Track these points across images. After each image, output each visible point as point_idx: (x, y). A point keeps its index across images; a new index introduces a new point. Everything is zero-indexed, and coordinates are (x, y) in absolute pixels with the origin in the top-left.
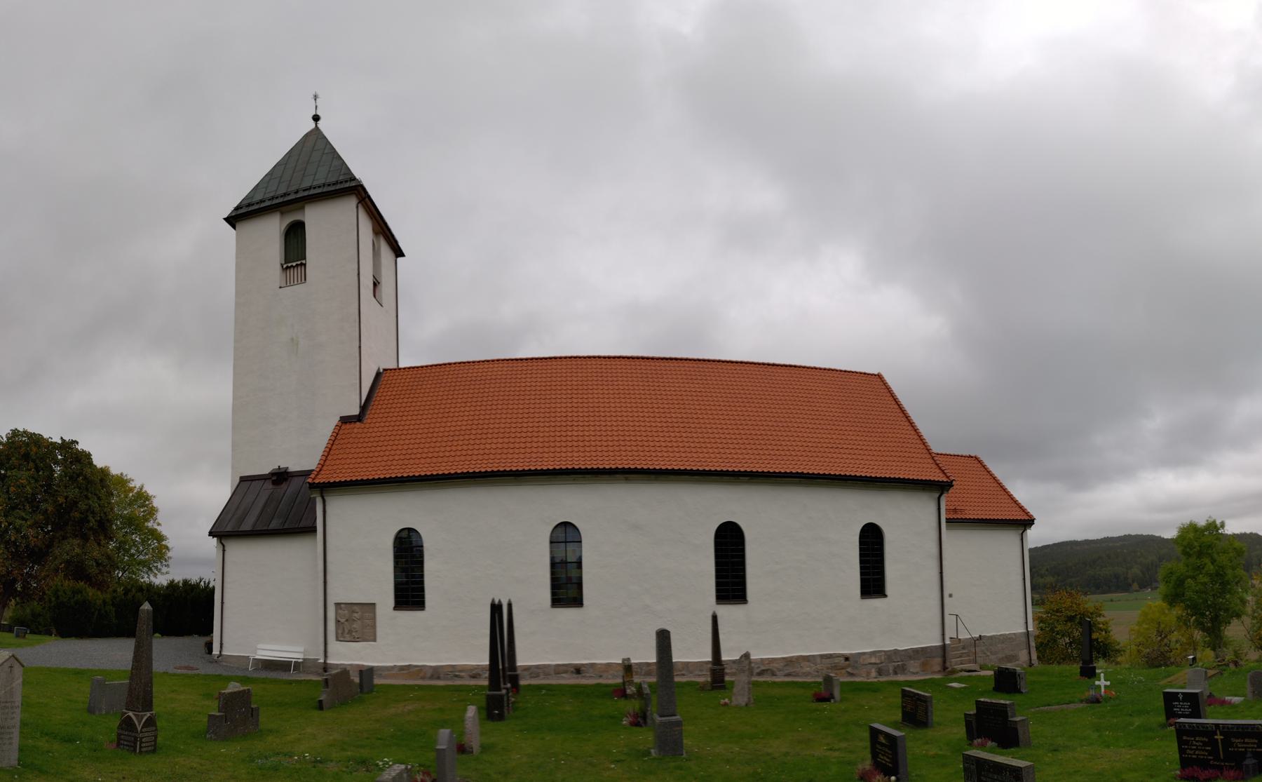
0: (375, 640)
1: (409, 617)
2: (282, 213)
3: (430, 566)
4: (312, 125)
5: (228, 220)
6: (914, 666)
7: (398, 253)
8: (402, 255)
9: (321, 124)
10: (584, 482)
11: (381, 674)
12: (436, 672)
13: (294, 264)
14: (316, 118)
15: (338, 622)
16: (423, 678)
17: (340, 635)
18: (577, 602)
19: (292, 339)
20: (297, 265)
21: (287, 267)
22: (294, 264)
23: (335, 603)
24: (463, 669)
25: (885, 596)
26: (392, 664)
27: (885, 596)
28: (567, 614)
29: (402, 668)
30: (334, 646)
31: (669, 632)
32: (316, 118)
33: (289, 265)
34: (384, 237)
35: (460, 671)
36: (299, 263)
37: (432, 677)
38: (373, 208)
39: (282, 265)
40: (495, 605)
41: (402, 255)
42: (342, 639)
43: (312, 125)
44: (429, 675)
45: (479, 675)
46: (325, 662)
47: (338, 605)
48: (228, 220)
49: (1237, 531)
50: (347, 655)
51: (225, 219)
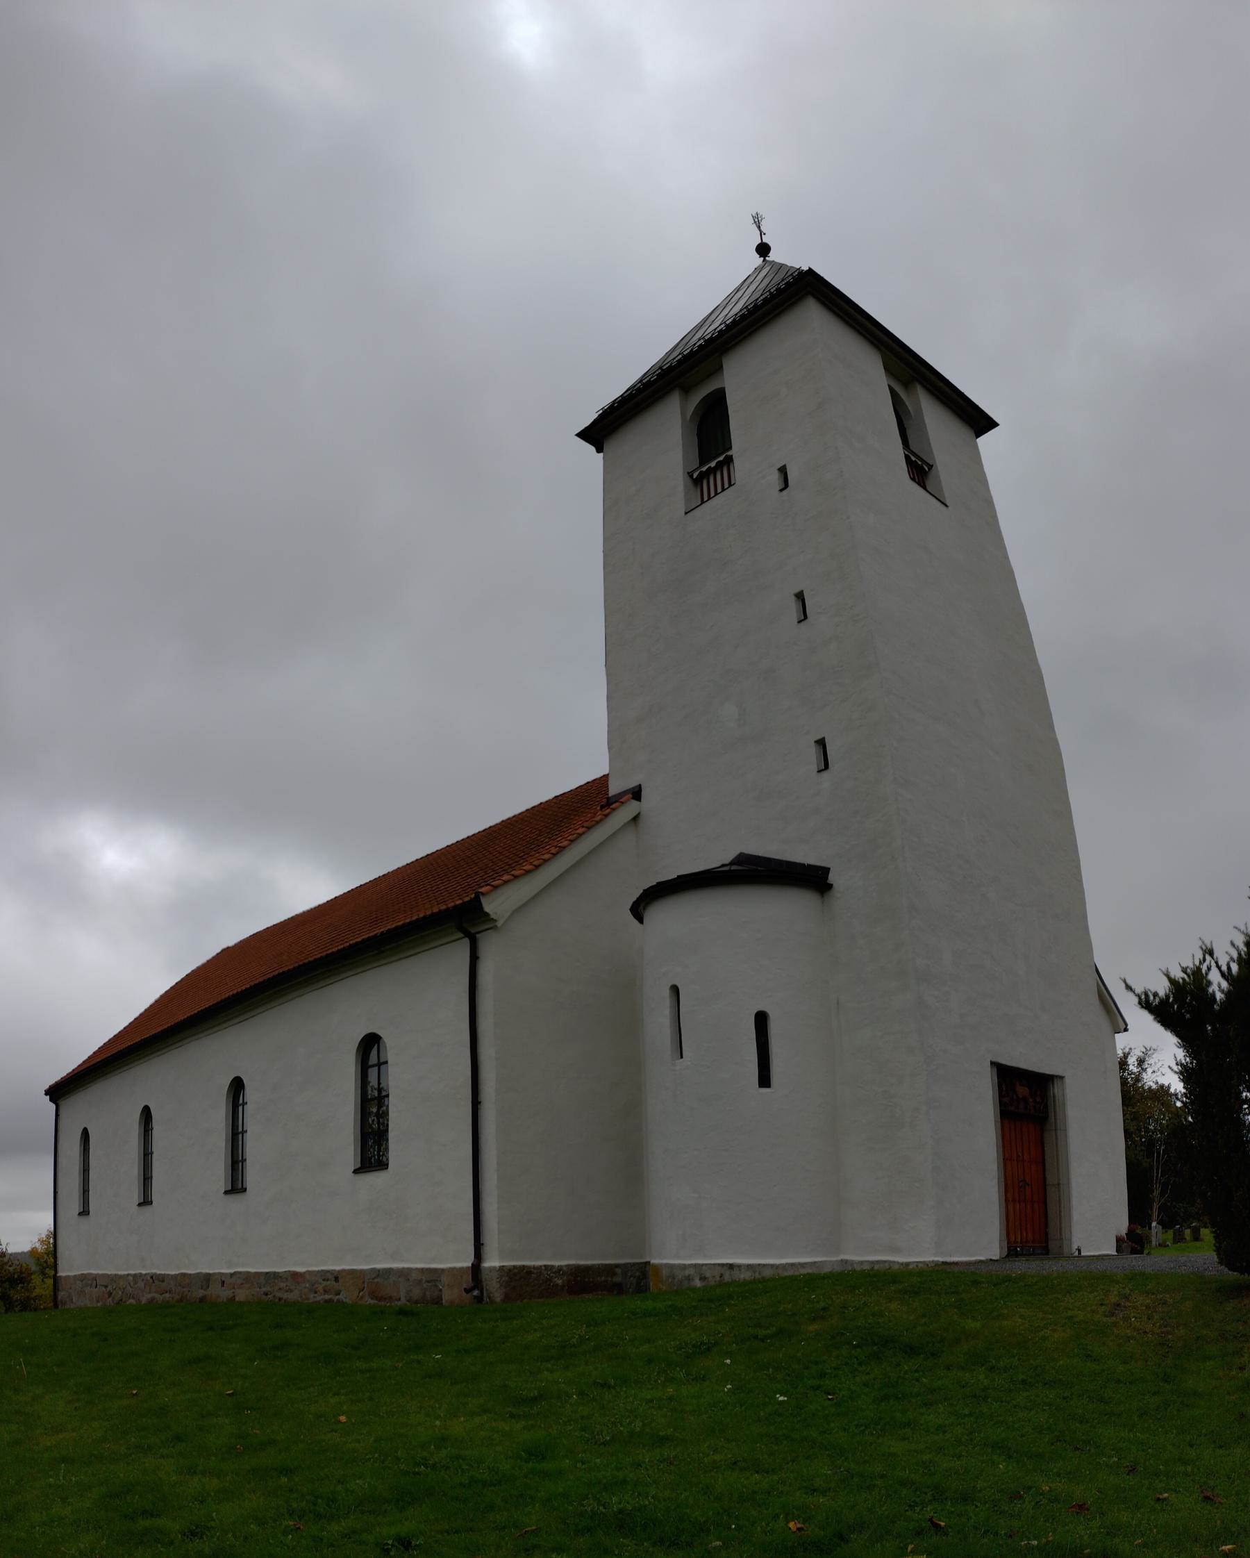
5: (584, 435)
7: (980, 422)
8: (989, 424)
13: (713, 464)
14: (763, 250)
18: (382, 1165)
20: (720, 465)
21: (704, 476)
22: (713, 464)
31: (741, 853)
34: (924, 386)
38: (874, 329)
39: (690, 475)
40: (1164, 1002)
41: (989, 424)
46: (476, 1268)
48: (584, 435)
49: (14, 1251)
50: (316, 1300)
51: (580, 435)
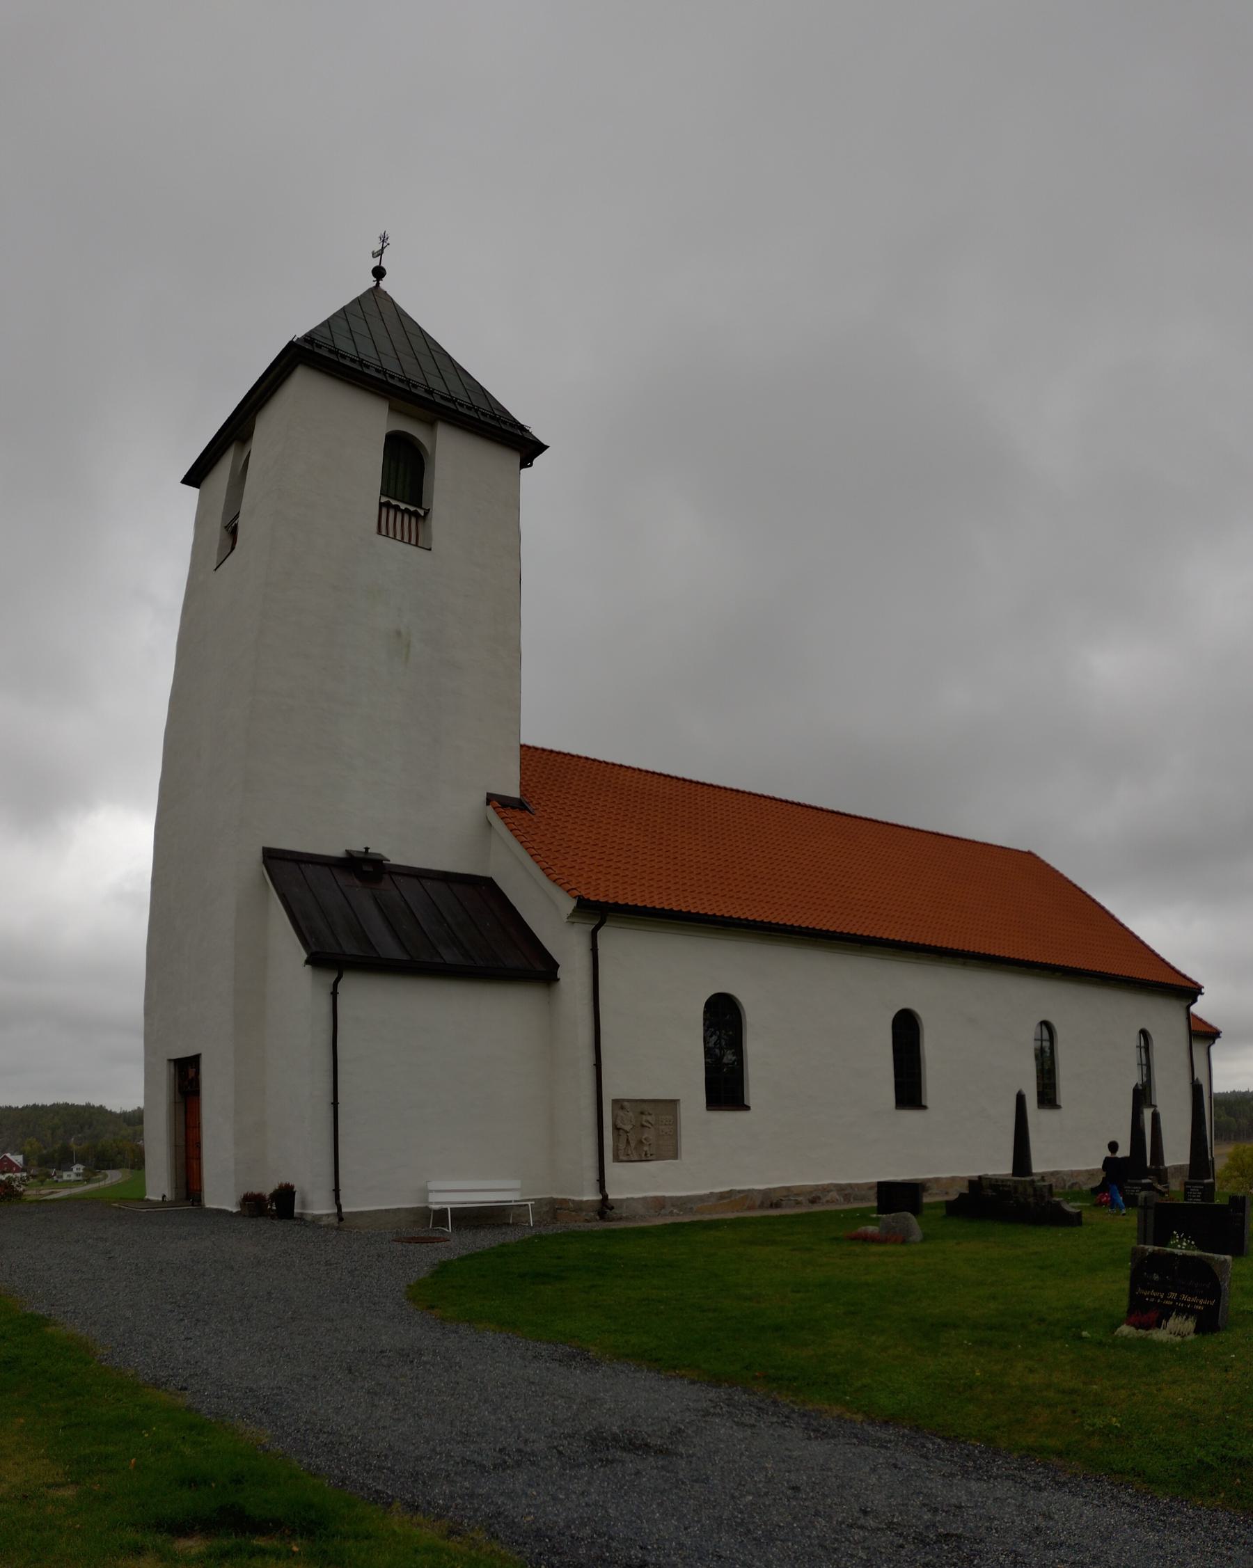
0: (675, 1157)
1: (727, 1119)
2: (392, 409)
3: (753, 1046)
4: (370, 282)
6: (324, 1218)
9: (384, 284)
10: (914, 961)
11: (691, 1208)
12: (771, 1199)
14: (379, 273)
15: (616, 1128)
16: (750, 1208)
17: (621, 1153)
19: (399, 633)
20: (407, 510)
22: (403, 506)
23: (613, 1100)
24: (799, 1191)
25: (922, 1107)
26: (707, 1192)
27: (922, 1107)
28: (910, 1117)
29: (722, 1196)
30: (614, 1170)
32: (379, 273)
33: (394, 502)
35: (798, 1195)
36: (394, 502)
37: (762, 1206)
42: (625, 1158)
43: (370, 282)
44: (758, 1203)
45: (819, 1198)
47: (615, 1102)
